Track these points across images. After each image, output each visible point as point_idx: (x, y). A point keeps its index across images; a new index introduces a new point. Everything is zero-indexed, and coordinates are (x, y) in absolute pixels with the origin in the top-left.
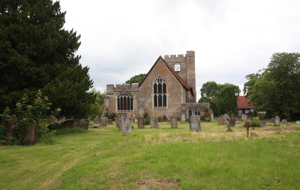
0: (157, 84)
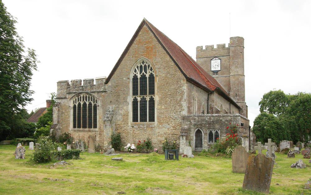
0: (139, 76)
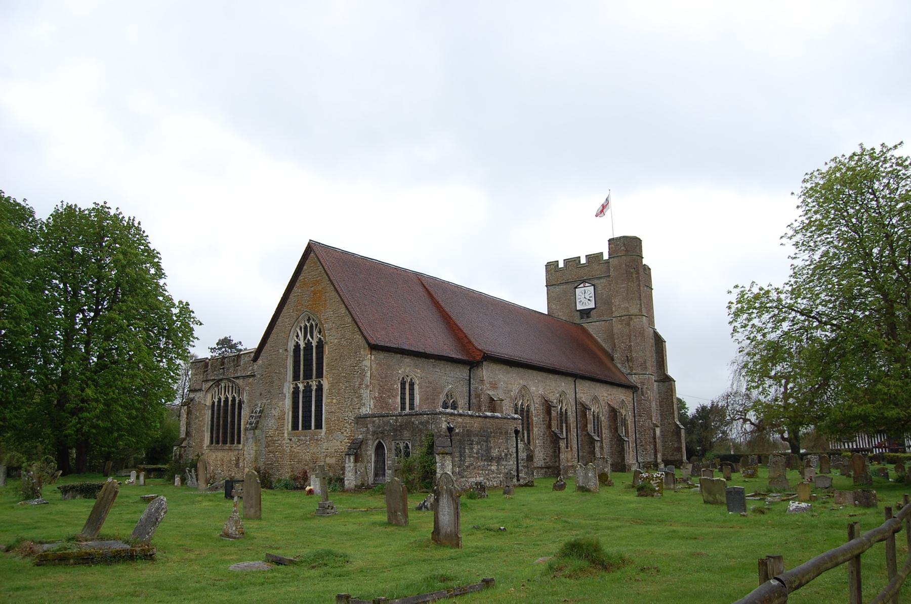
0: (302, 345)
